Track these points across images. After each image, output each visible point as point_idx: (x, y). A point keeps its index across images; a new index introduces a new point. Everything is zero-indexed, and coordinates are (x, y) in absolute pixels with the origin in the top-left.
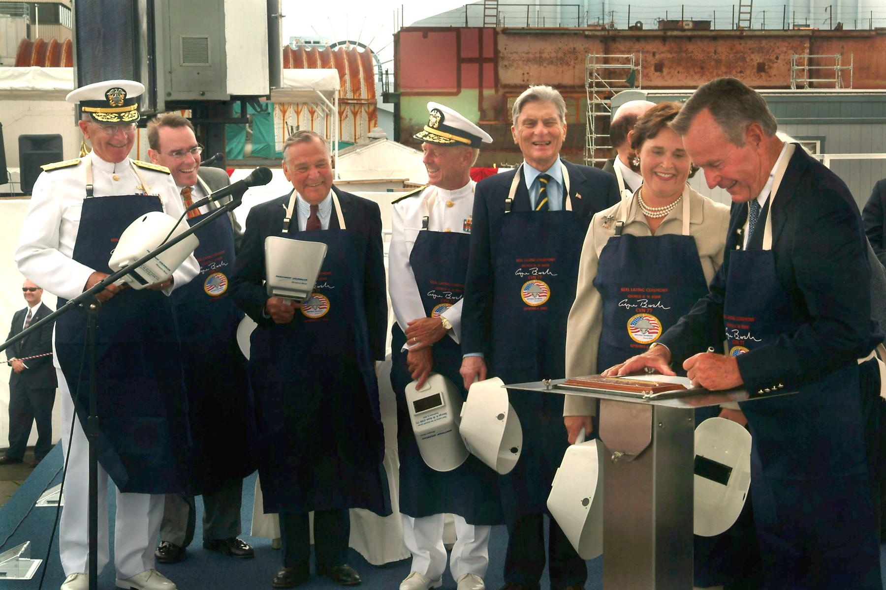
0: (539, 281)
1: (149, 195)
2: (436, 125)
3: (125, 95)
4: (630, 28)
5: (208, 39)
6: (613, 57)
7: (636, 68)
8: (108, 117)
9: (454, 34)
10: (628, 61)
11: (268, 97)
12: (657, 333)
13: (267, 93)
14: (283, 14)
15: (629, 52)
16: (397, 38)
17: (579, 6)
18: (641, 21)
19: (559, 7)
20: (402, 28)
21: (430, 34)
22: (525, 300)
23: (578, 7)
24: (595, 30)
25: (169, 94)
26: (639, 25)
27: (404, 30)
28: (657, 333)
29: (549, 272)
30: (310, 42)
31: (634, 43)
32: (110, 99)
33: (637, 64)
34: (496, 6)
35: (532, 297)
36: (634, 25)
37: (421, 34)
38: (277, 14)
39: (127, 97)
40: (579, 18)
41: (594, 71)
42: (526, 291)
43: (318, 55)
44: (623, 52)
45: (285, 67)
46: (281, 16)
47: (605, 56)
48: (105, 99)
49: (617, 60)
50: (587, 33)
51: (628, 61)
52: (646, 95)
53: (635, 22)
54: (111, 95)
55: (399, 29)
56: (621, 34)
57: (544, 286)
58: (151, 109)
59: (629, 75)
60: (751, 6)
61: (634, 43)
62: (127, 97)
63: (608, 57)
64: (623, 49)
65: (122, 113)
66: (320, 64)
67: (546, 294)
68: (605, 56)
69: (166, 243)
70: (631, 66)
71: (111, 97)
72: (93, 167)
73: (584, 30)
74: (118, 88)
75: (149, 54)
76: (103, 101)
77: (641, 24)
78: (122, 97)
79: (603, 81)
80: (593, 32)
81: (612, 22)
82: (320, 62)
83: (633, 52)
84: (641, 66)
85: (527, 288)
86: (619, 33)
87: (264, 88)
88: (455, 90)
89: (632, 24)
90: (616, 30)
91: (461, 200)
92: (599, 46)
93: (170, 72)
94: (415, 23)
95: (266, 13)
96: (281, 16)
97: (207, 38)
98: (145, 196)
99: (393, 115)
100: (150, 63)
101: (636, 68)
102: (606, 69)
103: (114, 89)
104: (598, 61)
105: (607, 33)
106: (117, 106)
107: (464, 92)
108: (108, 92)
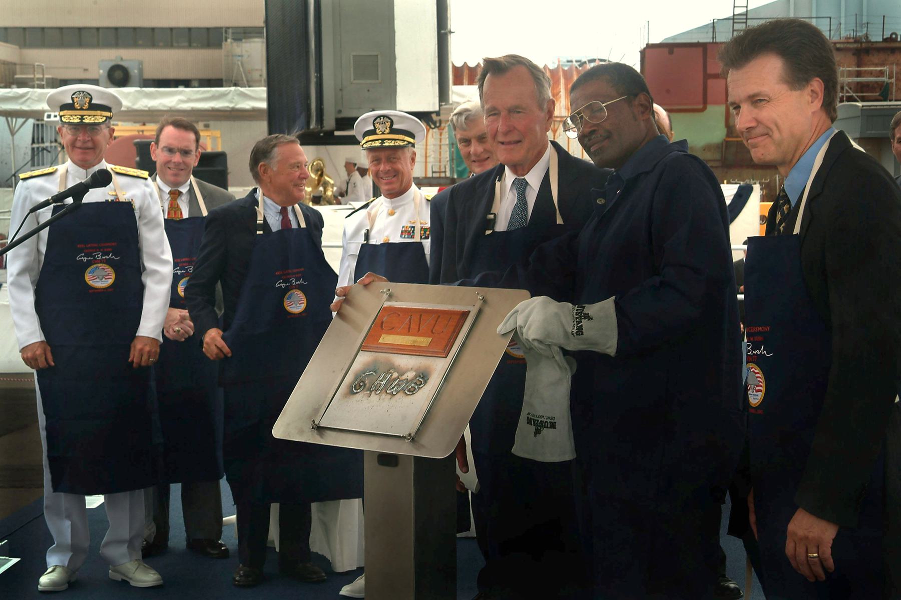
0: (104, 265)
1: (121, 200)
2: (388, 131)
3: (91, 99)
4: (885, 40)
5: (379, 57)
6: (865, 71)
7: (890, 81)
8: (72, 118)
9: (700, 49)
10: (881, 73)
11: (438, 113)
12: (303, 303)
13: (437, 109)
14: (452, 31)
15: (882, 65)
16: (643, 53)
17: (830, 18)
18: (896, 31)
19: (813, 16)
20: (647, 45)
21: (675, 50)
22: (288, 308)
23: (829, 19)
24: (848, 43)
25: (340, 112)
26: (894, 36)
27: (649, 46)
28: (303, 303)
29: (112, 256)
30: (571, 61)
31: (888, 55)
32: (75, 101)
33: (890, 77)
34: (745, 21)
35: (98, 280)
36: (889, 36)
37: (666, 50)
38: (447, 31)
39: (93, 102)
40: (830, 30)
41: (845, 84)
42: (91, 274)
43: (561, 72)
44: (877, 65)
45: (455, 83)
46: (451, 32)
47: (857, 69)
48: (71, 102)
49: (871, 73)
50: (838, 46)
51: (881, 73)
52: (860, 108)
53: (890, 33)
54: (77, 98)
55: (645, 46)
56: (874, 46)
57: (110, 270)
58: (318, 126)
59: (882, 89)
60: (747, 7)
61: (888, 55)
62: (93, 102)
63: (860, 71)
64: (876, 61)
65: (85, 115)
66: (563, 82)
67: (303, 302)
68: (857, 69)
69: (14, 240)
70: (885, 79)
71: (75, 100)
72: (68, 174)
73: (835, 43)
74: (83, 92)
75: (316, 72)
76: (69, 104)
77: (896, 35)
78: (87, 100)
79: (854, 95)
80: (845, 45)
81: (867, 34)
82: (563, 80)
83: (887, 64)
84: (894, 78)
85: (289, 298)
86: (872, 45)
87: (434, 104)
88: (701, 107)
89: (887, 35)
90: (870, 42)
91: (403, 207)
92: (852, 59)
93: (341, 90)
94: (665, 39)
95: (436, 29)
96: (451, 32)
97: (377, 56)
98: (116, 202)
99: (266, 116)
100: (317, 81)
101: (890, 81)
102: (858, 83)
103: (79, 92)
104: (850, 74)
105: (859, 45)
106: (81, 109)
107: (710, 108)
108: (73, 94)
